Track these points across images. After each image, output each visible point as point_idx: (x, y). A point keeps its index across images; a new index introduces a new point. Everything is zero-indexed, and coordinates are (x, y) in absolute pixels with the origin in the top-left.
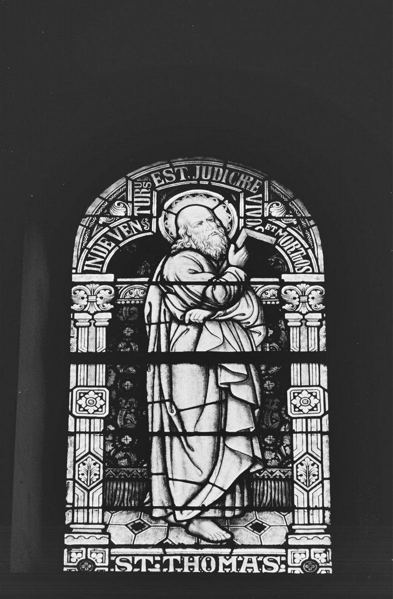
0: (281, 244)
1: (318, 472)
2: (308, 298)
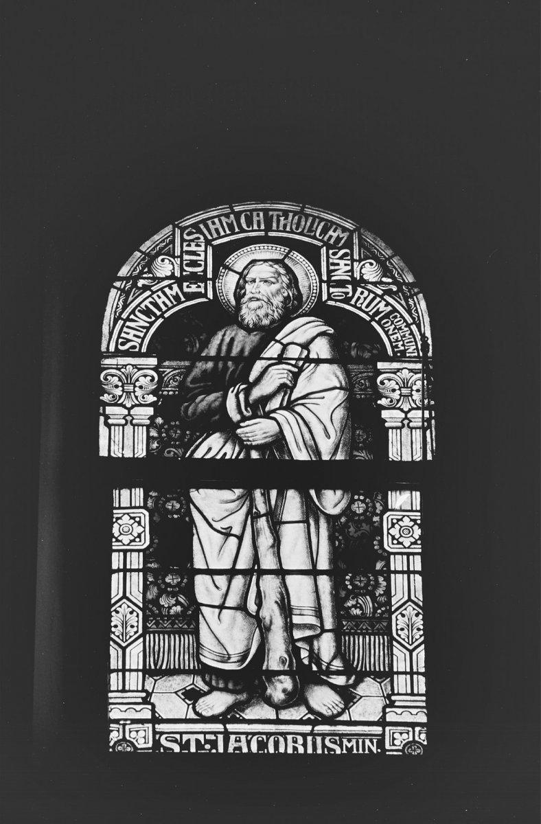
0: (402, 321)
1: (138, 622)
2: (412, 390)
